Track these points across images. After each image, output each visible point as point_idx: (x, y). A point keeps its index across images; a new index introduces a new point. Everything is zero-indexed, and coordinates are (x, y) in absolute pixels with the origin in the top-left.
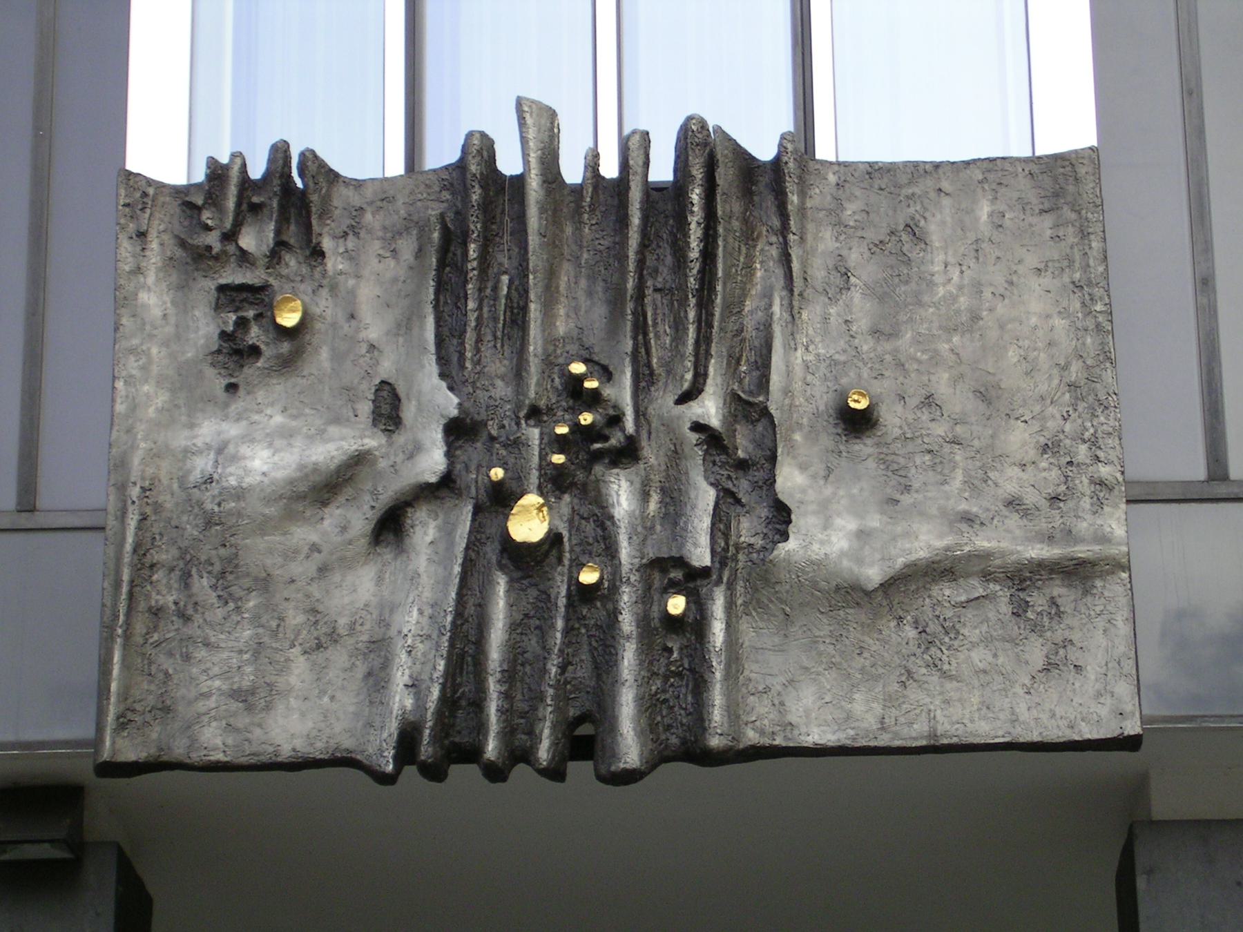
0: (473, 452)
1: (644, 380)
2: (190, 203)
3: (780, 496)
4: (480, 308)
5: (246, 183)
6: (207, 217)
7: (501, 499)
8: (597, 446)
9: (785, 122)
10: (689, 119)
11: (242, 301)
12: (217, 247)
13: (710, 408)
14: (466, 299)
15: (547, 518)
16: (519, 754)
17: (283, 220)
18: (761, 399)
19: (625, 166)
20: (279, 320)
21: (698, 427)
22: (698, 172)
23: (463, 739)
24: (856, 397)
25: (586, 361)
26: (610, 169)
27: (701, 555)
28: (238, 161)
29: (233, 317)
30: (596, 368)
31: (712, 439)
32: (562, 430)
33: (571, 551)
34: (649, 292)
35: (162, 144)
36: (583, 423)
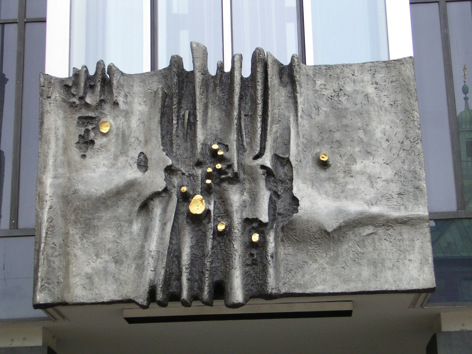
0: (176, 180)
1: (241, 148)
2: (67, 86)
3: (295, 195)
4: (178, 123)
5: (89, 78)
6: (73, 90)
7: (186, 198)
8: (224, 176)
9: (293, 50)
10: (257, 49)
11: (88, 123)
12: (78, 102)
13: (267, 160)
14: (173, 120)
15: (204, 204)
16: (195, 297)
17: (102, 91)
18: (287, 156)
19: (233, 68)
20: (101, 130)
21: (263, 167)
22: (260, 69)
23: (173, 289)
24: (323, 156)
25: (219, 144)
26: (227, 69)
27: (265, 218)
28: (85, 69)
29: (83, 129)
30: (223, 146)
31: (269, 173)
32: (210, 170)
33: (214, 215)
34: (243, 116)
35: (58, 63)
36: (218, 168)
